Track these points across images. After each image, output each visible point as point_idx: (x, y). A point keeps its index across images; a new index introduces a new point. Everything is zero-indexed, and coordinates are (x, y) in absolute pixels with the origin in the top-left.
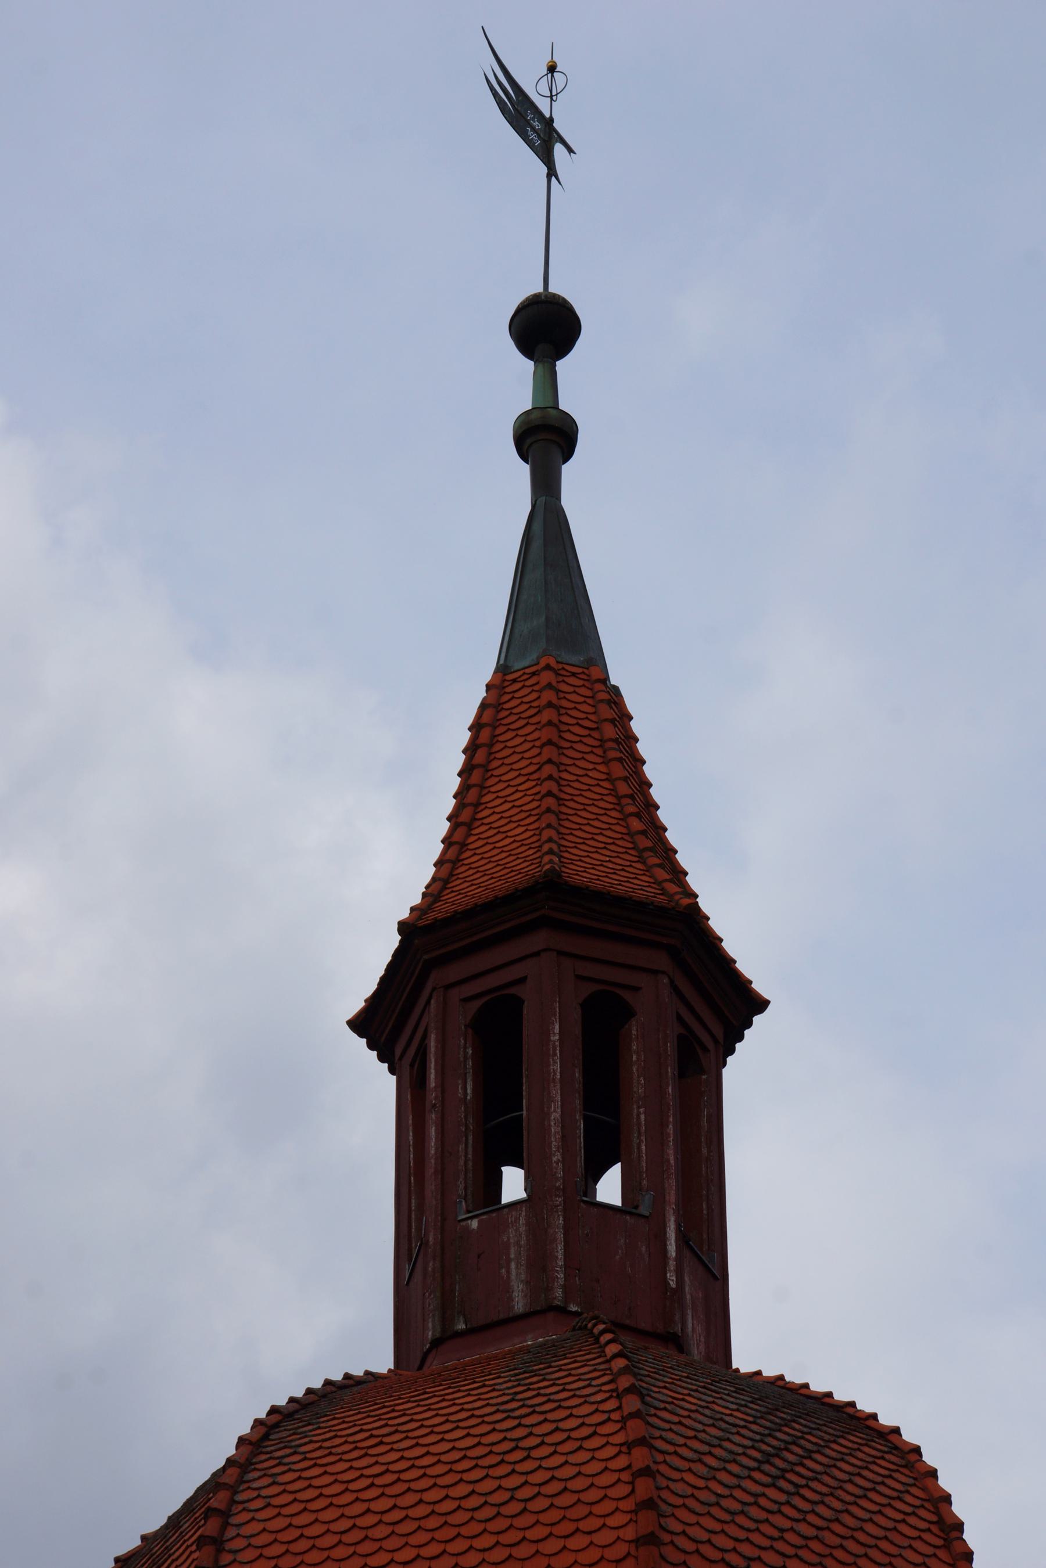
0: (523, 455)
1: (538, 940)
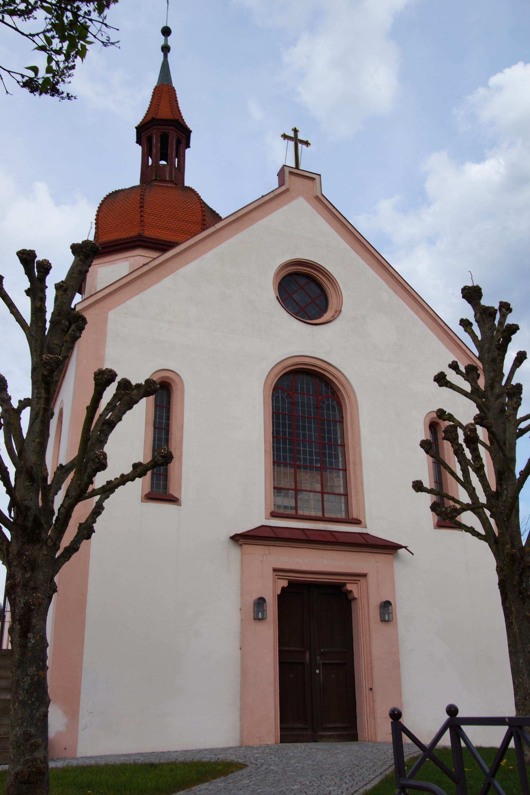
0: (162, 51)
1: (172, 128)
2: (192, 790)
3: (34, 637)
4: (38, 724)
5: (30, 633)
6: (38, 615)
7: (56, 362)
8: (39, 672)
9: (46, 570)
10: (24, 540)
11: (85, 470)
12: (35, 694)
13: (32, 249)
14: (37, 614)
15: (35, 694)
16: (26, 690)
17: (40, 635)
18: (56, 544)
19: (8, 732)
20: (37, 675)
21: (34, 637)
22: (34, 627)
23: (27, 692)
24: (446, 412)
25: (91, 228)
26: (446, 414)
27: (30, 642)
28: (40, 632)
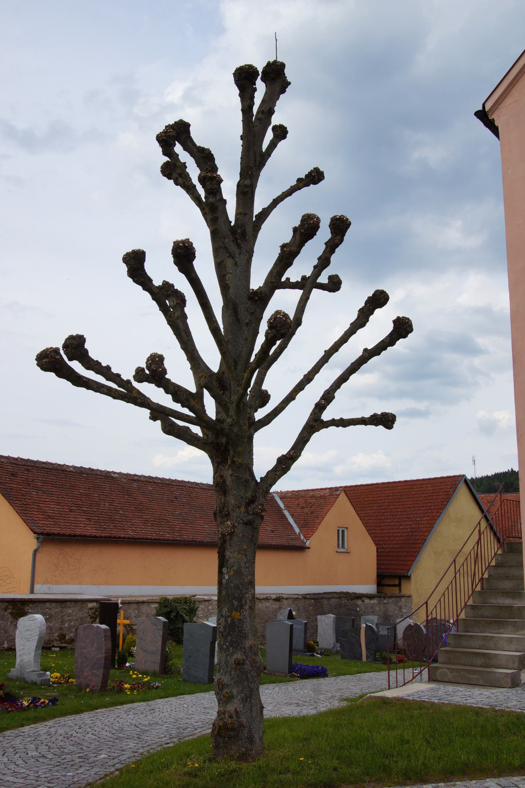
2: (456, 785)
3: (228, 573)
4: (233, 673)
5: (224, 568)
6: (232, 546)
7: (133, 258)
8: (231, 613)
9: (235, 492)
10: (219, 460)
11: (234, 366)
12: (229, 638)
13: (177, 120)
14: (230, 545)
15: (229, 638)
16: (222, 632)
17: (234, 570)
18: (234, 461)
19: (483, 646)
20: (230, 616)
21: (228, 573)
22: (227, 560)
23: (222, 636)
24: (255, 85)
25: (276, 40)
26: (254, 87)
27: (225, 578)
28: (233, 567)
